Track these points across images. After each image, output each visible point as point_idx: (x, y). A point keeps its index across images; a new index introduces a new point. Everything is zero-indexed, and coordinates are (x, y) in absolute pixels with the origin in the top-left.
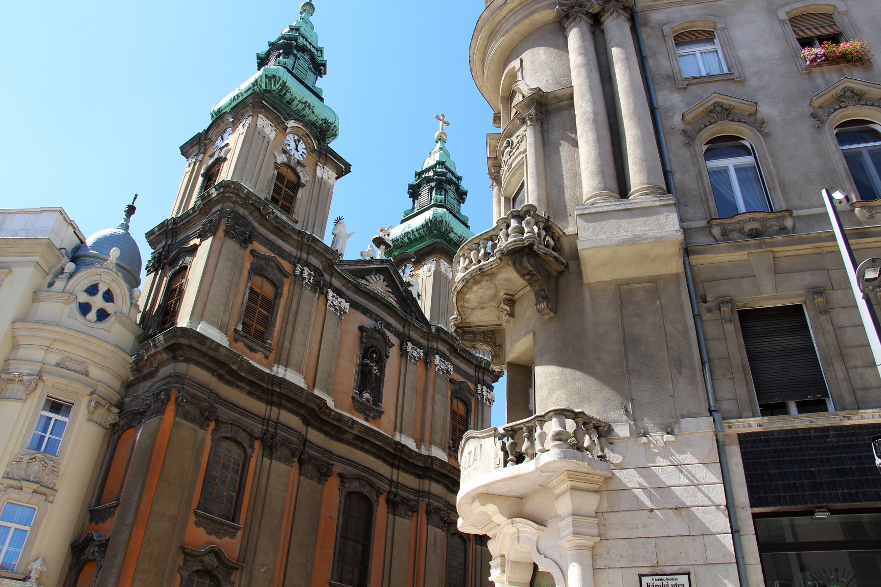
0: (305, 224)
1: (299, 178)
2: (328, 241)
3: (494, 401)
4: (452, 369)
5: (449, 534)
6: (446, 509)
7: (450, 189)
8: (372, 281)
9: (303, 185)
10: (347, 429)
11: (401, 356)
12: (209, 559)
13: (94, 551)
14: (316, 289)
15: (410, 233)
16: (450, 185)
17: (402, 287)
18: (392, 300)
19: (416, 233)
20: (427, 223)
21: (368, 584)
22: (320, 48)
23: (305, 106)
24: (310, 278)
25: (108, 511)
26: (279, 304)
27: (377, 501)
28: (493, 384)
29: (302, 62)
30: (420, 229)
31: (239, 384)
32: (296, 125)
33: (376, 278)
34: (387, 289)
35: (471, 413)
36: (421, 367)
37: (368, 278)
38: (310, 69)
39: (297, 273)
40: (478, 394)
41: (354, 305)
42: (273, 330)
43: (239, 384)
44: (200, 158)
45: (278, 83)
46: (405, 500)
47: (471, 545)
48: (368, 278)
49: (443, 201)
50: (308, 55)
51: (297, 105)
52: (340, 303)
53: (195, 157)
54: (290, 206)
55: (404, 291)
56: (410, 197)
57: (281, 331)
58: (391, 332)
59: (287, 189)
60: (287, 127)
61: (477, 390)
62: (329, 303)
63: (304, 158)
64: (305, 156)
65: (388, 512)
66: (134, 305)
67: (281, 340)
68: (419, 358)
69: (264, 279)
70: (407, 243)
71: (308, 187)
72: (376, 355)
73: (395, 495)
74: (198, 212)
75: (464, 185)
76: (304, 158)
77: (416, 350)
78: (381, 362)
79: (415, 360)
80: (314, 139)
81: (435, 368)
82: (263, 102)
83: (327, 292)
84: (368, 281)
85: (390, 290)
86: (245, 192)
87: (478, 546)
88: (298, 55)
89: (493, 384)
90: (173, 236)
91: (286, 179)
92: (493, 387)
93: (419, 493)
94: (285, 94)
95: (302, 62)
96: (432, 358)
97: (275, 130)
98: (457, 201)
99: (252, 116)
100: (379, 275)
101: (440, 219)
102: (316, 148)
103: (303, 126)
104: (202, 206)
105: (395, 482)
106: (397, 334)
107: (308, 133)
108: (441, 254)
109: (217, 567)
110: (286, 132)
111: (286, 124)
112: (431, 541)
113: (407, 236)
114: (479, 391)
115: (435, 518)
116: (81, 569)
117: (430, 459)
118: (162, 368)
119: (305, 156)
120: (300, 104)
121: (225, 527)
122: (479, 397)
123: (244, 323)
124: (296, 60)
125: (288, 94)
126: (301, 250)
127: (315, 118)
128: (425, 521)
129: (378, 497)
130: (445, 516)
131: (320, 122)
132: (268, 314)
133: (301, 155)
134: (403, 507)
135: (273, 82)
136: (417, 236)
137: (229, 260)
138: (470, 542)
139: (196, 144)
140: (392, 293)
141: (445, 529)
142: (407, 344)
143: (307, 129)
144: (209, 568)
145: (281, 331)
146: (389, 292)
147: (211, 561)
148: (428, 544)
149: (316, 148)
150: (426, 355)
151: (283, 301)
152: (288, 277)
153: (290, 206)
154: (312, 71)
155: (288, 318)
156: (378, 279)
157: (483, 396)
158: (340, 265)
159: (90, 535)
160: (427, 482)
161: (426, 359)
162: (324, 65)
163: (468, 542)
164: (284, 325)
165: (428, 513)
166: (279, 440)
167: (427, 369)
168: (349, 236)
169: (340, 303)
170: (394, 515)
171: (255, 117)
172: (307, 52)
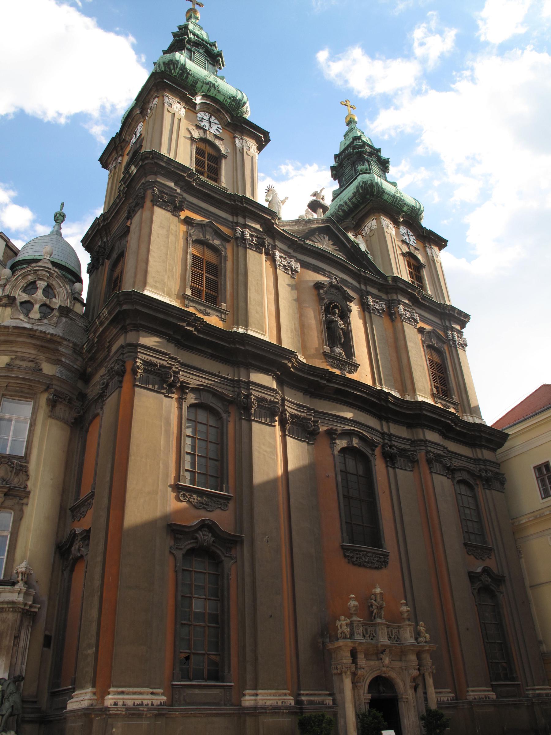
0: (235, 180)
1: (218, 150)
2: (261, 199)
3: (466, 346)
4: (418, 318)
5: (455, 482)
6: (445, 455)
7: (372, 160)
8: (317, 241)
9: (225, 157)
10: (325, 382)
11: (364, 311)
12: (204, 535)
13: (79, 547)
14: (261, 250)
15: (343, 206)
16: (371, 157)
17: (349, 243)
18: (341, 256)
19: (349, 204)
20: (358, 190)
21: (383, 543)
22: (213, 43)
23: (210, 86)
24: (253, 240)
25: (86, 503)
26: (225, 268)
27: (373, 455)
28: (462, 330)
29: (197, 54)
30: (352, 198)
31: (199, 347)
32: (205, 101)
33: (320, 238)
34: (334, 247)
35: (447, 359)
36: (386, 320)
37: (313, 238)
38: (208, 61)
39: (238, 235)
40: (450, 340)
41: (304, 265)
42: (225, 293)
43: (199, 347)
44: (119, 161)
45: (177, 67)
46: (403, 452)
47: (479, 490)
48: (313, 238)
49: (368, 169)
50: (202, 49)
51: (202, 87)
52: (289, 263)
53: (114, 163)
54: (216, 177)
55: (351, 247)
56: (335, 180)
57: (233, 293)
58: (348, 287)
59: (209, 162)
60: (196, 104)
61: (447, 337)
62: (278, 263)
63: (219, 132)
64: (221, 131)
65: (387, 466)
66: (76, 298)
67: (235, 302)
68: (382, 310)
69: (205, 247)
70: (342, 217)
71: (230, 158)
72: (339, 310)
73: (391, 447)
74: (124, 198)
75: (384, 154)
76: (219, 132)
77: (377, 302)
78: (345, 315)
79: (379, 312)
80: (226, 113)
81: (401, 318)
82: (165, 80)
83: (274, 254)
84: (313, 241)
85: (338, 249)
86: (165, 160)
87: (487, 491)
88: (193, 50)
89: (462, 330)
90: (106, 233)
91: (207, 153)
92: (463, 332)
93: (413, 442)
94: (187, 77)
95: (197, 54)
96: (395, 309)
97: (185, 108)
98: (382, 170)
99: (158, 97)
100: (322, 235)
101: (369, 182)
102: (229, 121)
103: (211, 102)
104: (126, 189)
105: (387, 434)
106: (354, 289)
107: (218, 108)
108: (379, 213)
109: (214, 542)
110: (195, 109)
111: (194, 101)
112: (438, 489)
113: (341, 209)
114: (450, 337)
115: (437, 466)
116: (72, 571)
117: (418, 405)
118: (113, 345)
119: (221, 131)
120: (205, 86)
121: (214, 499)
122: (451, 343)
123: (192, 288)
124: (191, 54)
125: (190, 77)
126: (237, 216)
127: (223, 97)
128: (428, 472)
129: (373, 450)
130: (447, 462)
131: (229, 101)
132: (216, 279)
133: (217, 129)
134: (402, 459)
135: (172, 68)
136: (351, 206)
137: (163, 228)
138: (478, 487)
139: (113, 150)
140: (339, 251)
141: (450, 477)
142: (367, 298)
143: (216, 104)
144: (205, 544)
145: (233, 293)
146: (336, 250)
147: (206, 537)
148: (437, 494)
149: (229, 121)
150: (389, 307)
151: (229, 265)
152: (228, 241)
153: (216, 177)
154: (210, 63)
155: (238, 280)
156: (322, 238)
157: (455, 341)
158: (282, 226)
159: (73, 531)
160: (420, 431)
161: (390, 311)
162: (220, 55)
163: (476, 488)
164: (235, 287)
165: (429, 462)
166: (254, 399)
167: (392, 320)
168: (283, 202)
169: (289, 263)
170: (394, 468)
171: (161, 98)
172: (201, 46)
